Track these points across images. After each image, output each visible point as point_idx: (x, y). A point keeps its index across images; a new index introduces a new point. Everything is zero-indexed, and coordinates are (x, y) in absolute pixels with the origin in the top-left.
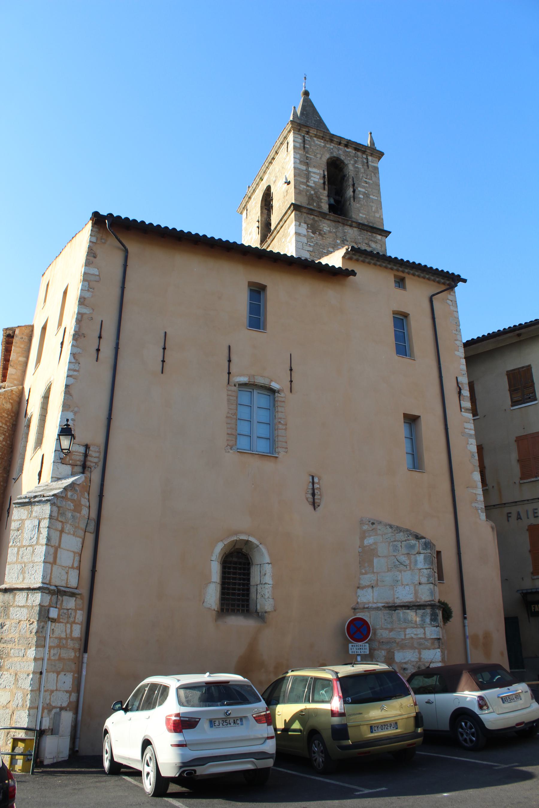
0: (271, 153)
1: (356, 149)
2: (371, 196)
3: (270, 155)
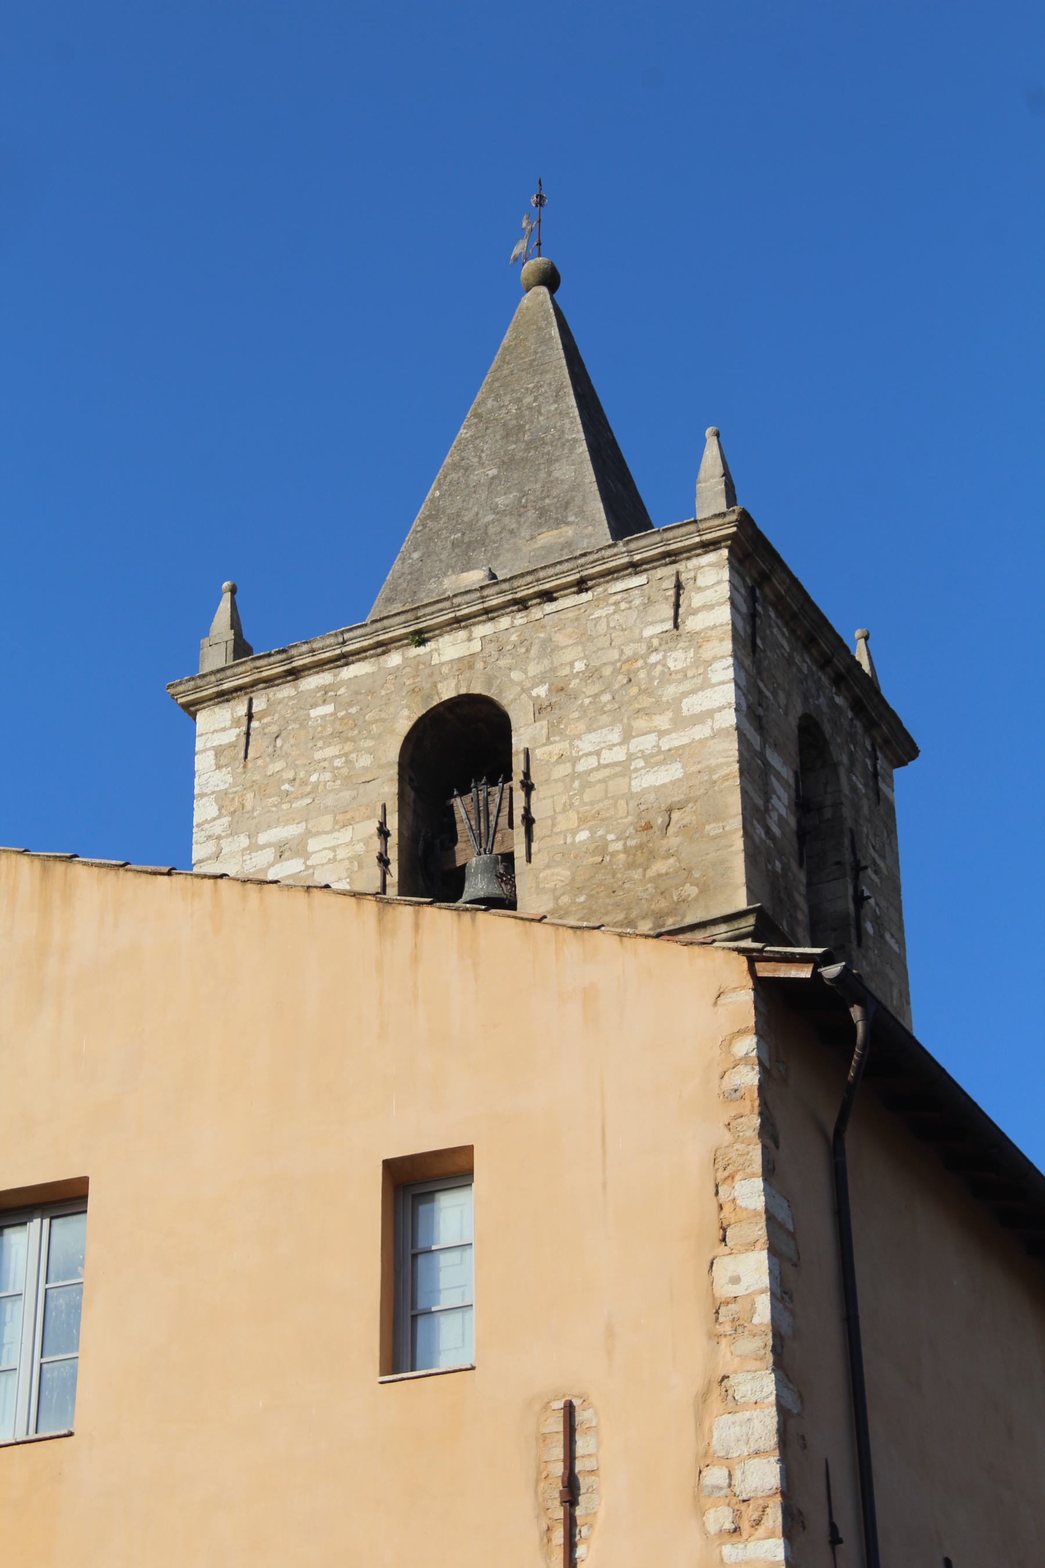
0: (551, 571)
1: (858, 706)
2: (888, 936)
3: (542, 574)
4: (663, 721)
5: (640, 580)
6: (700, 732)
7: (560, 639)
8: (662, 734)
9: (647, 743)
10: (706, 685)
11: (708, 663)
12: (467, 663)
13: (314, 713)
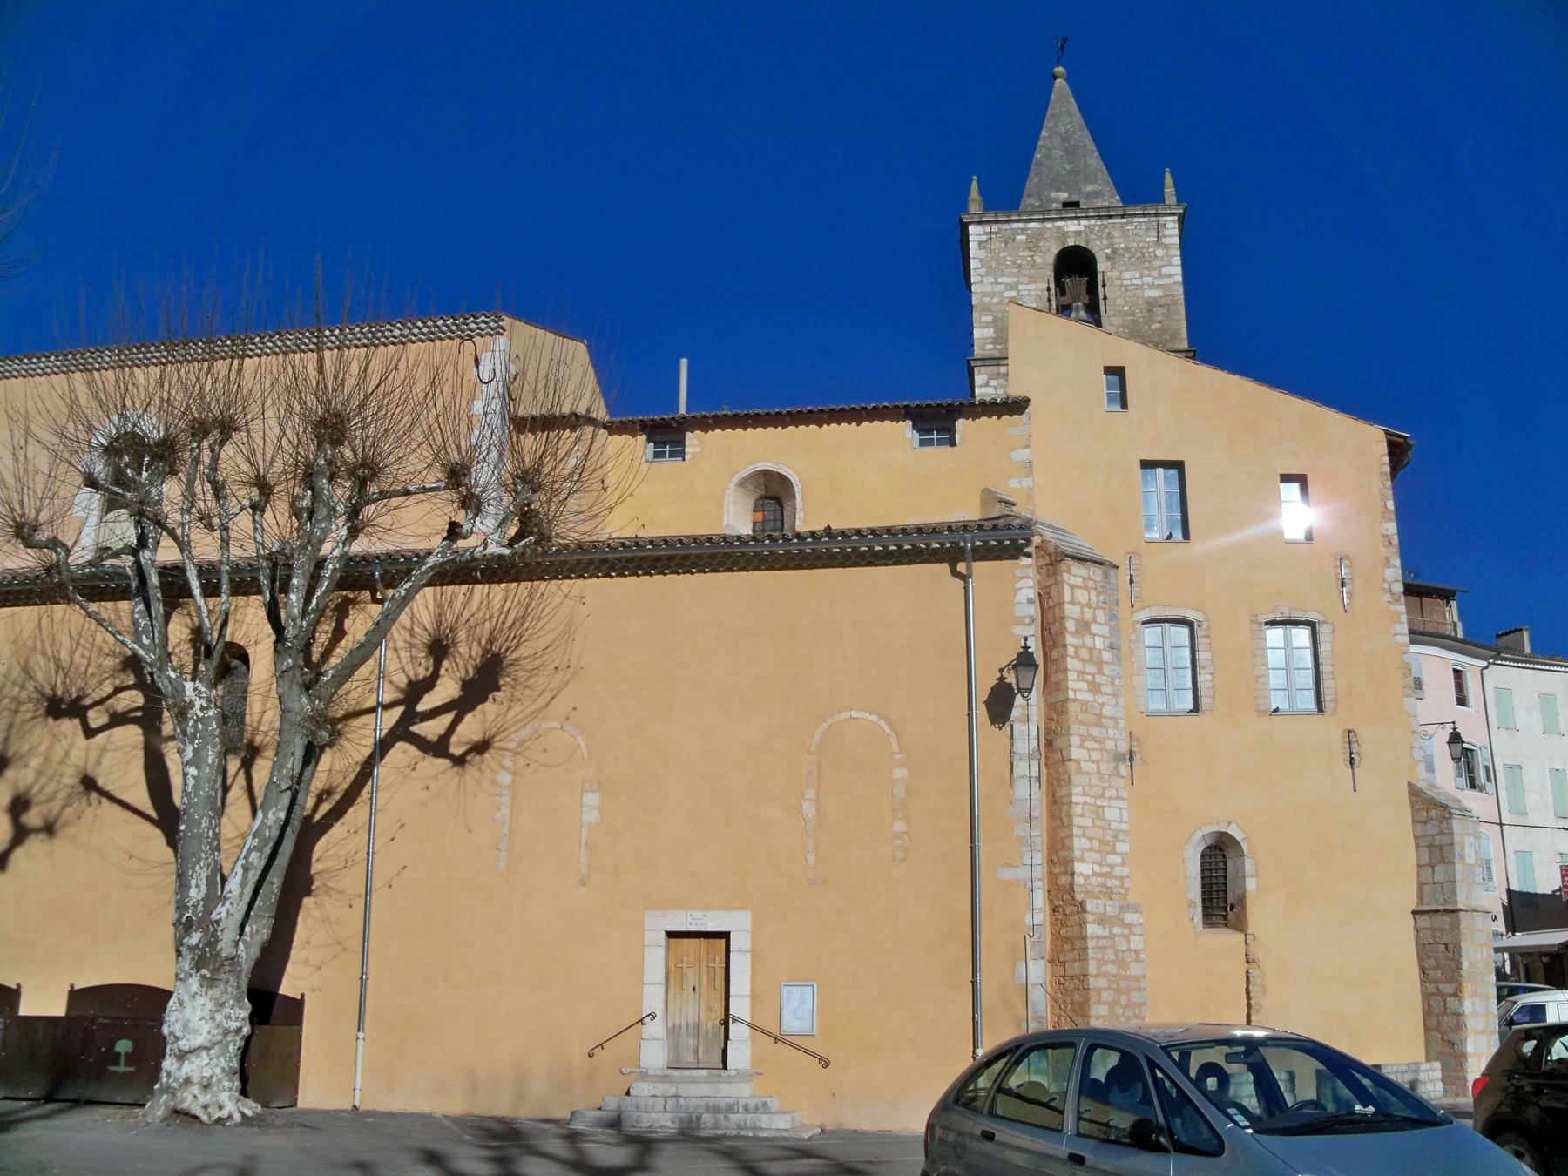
4: (1155, 274)
5: (1145, 219)
6: (1169, 281)
7: (1115, 233)
8: (1155, 278)
9: (1150, 280)
10: (1170, 264)
11: (1171, 257)
12: (1078, 233)
13: (1018, 237)
